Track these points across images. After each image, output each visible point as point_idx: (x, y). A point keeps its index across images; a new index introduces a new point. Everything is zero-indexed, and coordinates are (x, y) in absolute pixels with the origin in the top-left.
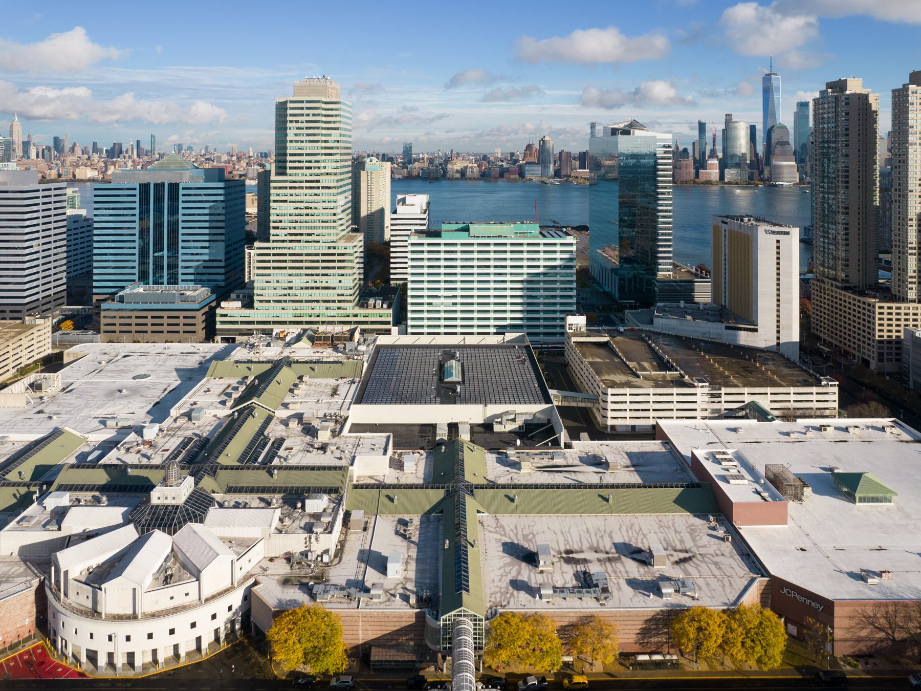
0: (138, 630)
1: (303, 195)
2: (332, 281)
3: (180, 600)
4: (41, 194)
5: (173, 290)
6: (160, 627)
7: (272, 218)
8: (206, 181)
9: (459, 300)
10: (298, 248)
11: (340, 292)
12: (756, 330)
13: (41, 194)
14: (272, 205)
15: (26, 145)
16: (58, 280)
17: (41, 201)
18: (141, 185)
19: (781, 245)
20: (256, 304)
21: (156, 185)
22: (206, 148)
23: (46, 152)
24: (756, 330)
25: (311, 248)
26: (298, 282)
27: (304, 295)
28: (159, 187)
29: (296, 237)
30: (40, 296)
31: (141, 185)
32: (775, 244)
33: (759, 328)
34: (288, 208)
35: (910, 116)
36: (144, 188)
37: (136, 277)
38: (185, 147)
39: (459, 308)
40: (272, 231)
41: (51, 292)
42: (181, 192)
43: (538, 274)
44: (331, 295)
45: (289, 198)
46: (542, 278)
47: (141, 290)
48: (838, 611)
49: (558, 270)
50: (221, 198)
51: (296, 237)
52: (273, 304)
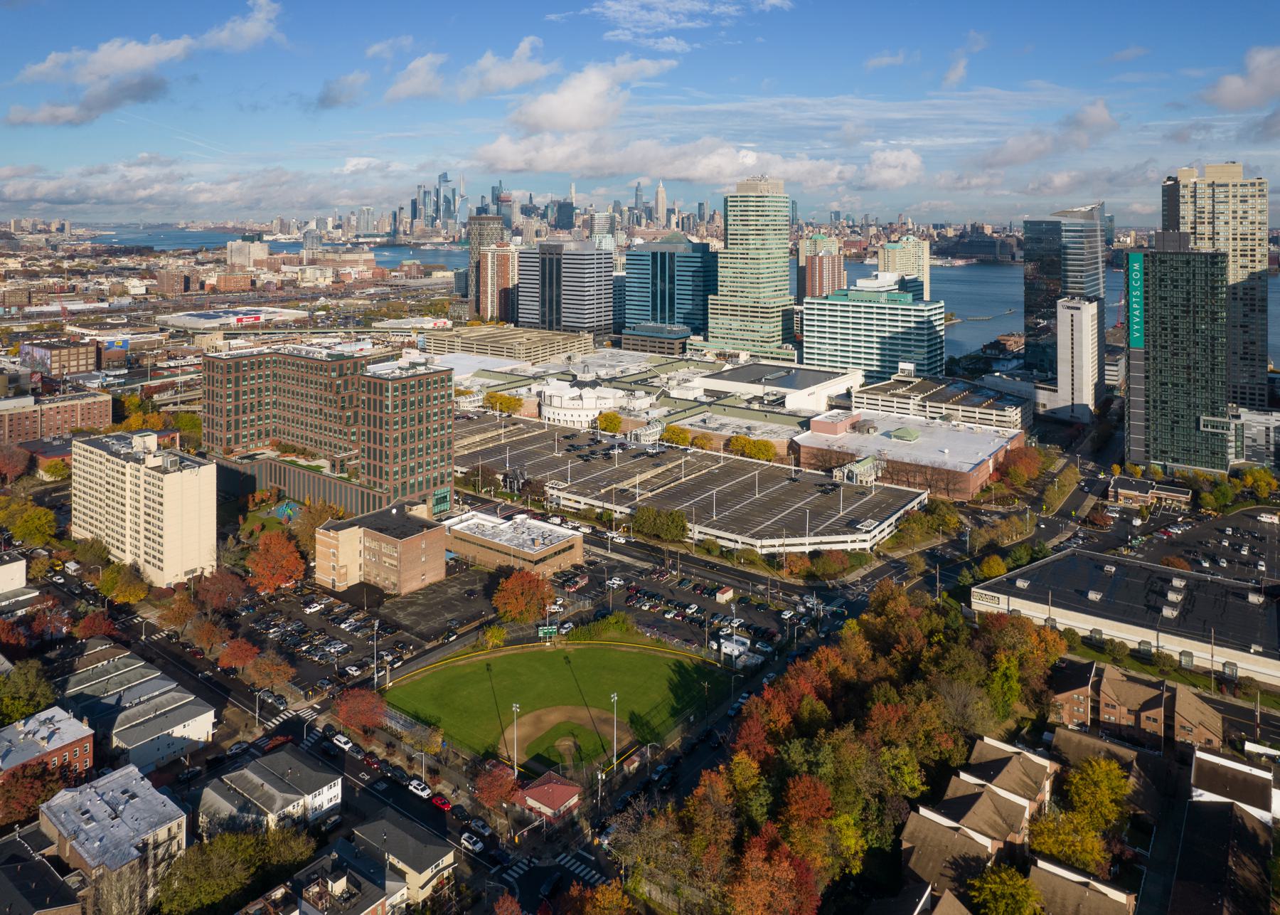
0: (562, 412)
1: (739, 264)
2: (756, 326)
3: (576, 406)
4: (595, 257)
5: (668, 327)
6: (569, 413)
7: (719, 279)
8: (694, 251)
9: (839, 348)
10: (735, 301)
11: (762, 334)
12: (1056, 391)
13: (595, 257)
14: (719, 269)
15: (670, 212)
16: (607, 318)
17: (595, 261)
18: (653, 253)
19: (1074, 318)
20: (710, 339)
21: (661, 254)
22: (866, 216)
23: (685, 220)
24: (1056, 391)
25: (743, 302)
26: (735, 325)
27: (739, 335)
28: (663, 255)
29: (734, 294)
30: (595, 324)
31: (653, 253)
32: (1070, 318)
33: (1058, 388)
34: (728, 272)
35: (1182, 207)
36: (654, 255)
37: (650, 318)
38: (843, 216)
39: (839, 353)
40: (719, 288)
41: (603, 323)
42: (676, 259)
43: (898, 333)
44: (756, 336)
45: (729, 265)
46: (900, 336)
47: (651, 324)
48: (802, 450)
49: (913, 331)
50: (699, 265)
51: (734, 294)
52: (720, 339)
